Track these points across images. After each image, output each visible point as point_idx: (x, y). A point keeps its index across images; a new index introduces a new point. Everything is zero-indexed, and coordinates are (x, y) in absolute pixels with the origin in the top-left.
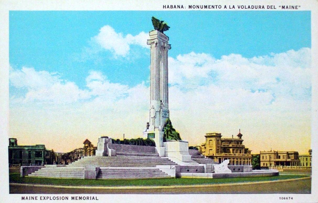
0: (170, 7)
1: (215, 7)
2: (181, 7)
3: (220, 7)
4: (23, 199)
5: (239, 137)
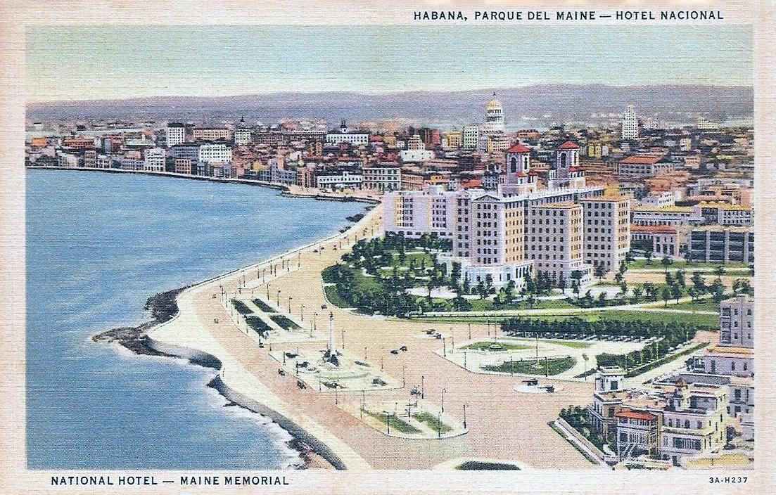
0: (430, 15)
2: (669, 16)
5: (598, 300)
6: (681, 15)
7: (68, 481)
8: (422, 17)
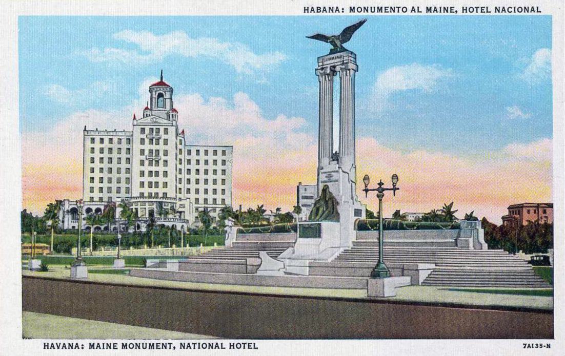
1: (396, 9)
3: (405, 10)
4: (152, 347)
6: (510, 10)
7: (192, 346)
8: (310, 11)
